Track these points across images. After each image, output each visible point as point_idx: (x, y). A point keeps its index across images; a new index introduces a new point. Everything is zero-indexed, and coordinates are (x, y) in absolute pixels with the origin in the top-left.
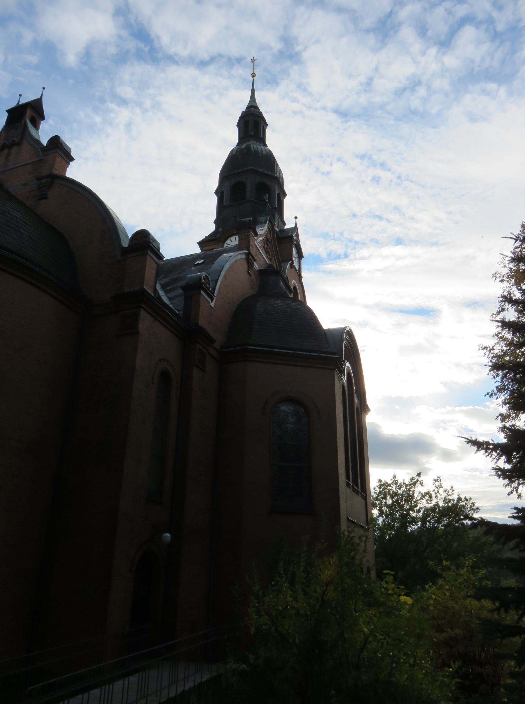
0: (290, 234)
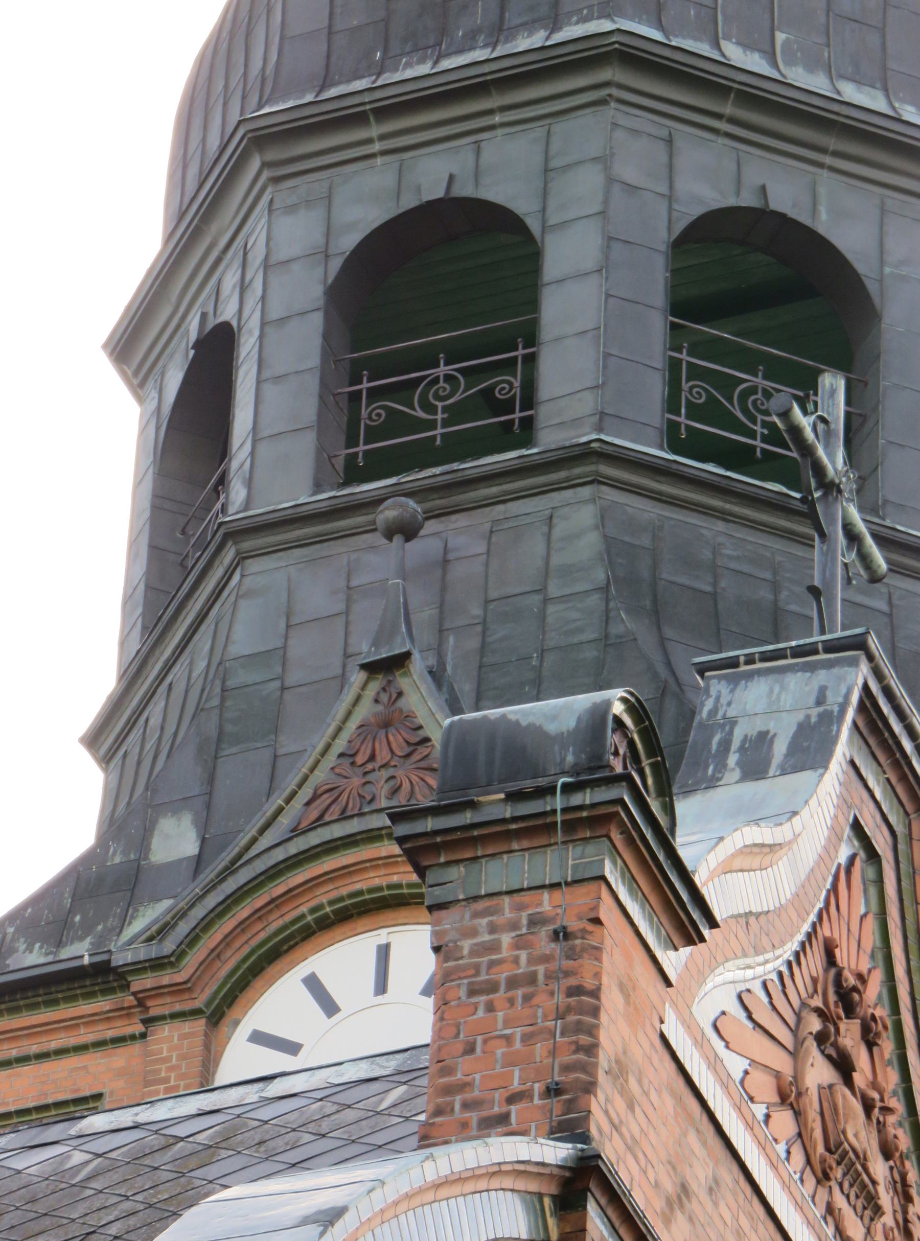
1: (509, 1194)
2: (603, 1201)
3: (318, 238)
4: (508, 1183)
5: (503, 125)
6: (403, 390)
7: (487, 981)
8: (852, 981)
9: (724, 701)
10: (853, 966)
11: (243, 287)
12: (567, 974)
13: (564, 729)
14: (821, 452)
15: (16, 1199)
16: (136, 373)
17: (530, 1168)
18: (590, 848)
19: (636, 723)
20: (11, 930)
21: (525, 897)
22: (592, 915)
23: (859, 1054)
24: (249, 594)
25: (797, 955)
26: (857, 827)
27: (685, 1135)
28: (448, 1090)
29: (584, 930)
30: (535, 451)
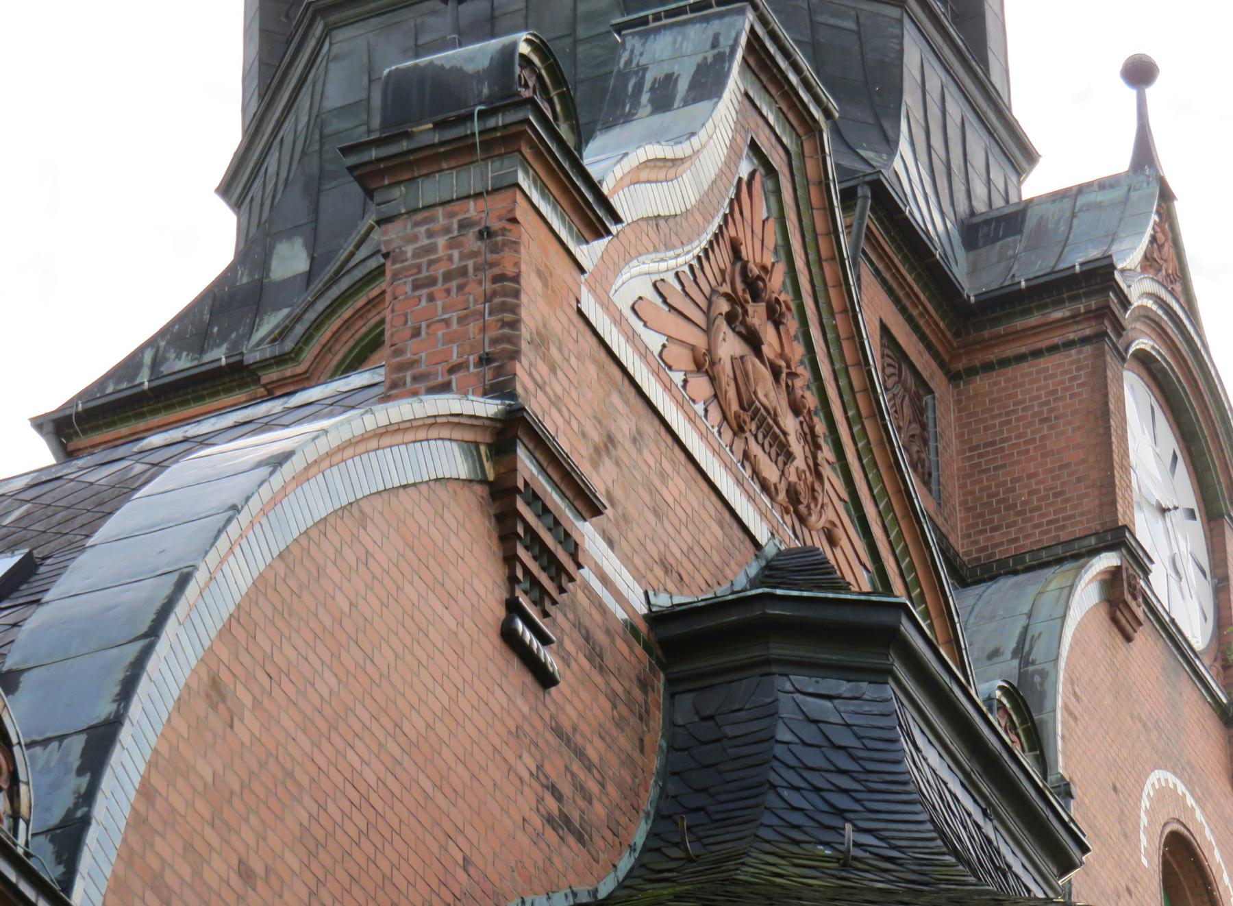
0: (1078, 258)
1: (448, 443)
2: (531, 446)
4: (445, 433)
7: (427, 277)
8: (756, 271)
9: (637, 52)
10: (758, 260)
12: (492, 265)
13: (480, 68)
15: (88, 505)
17: (463, 420)
18: (507, 162)
19: (542, 61)
20: (163, 344)
22: (510, 216)
23: (766, 330)
24: (337, 58)
25: (706, 251)
26: (754, 147)
27: (609, 395)
28: (401, 367)
29: (504, 229)
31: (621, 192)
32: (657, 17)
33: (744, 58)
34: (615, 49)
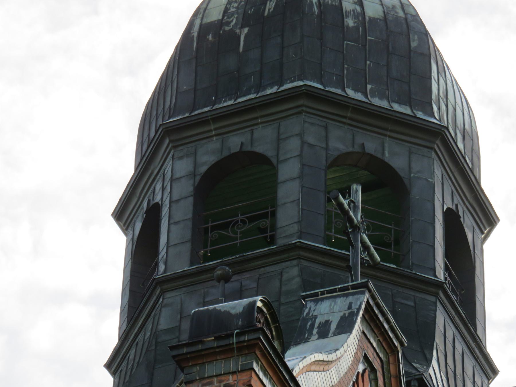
3: (191, 168)
5: (262, 123)
6: (225, 226)
9: (312, 309)
11: (163, 189)
13: (238, 312)
14: (351, 213)
16: (124, 225)
21: (223, 378)
22: (249, 384)
24: (166, 306)
26: (366, 357)
30: (275, 247)
31: (302, 375)
32: (323, 293)
33: (363, 315)
34: (304, 306)
